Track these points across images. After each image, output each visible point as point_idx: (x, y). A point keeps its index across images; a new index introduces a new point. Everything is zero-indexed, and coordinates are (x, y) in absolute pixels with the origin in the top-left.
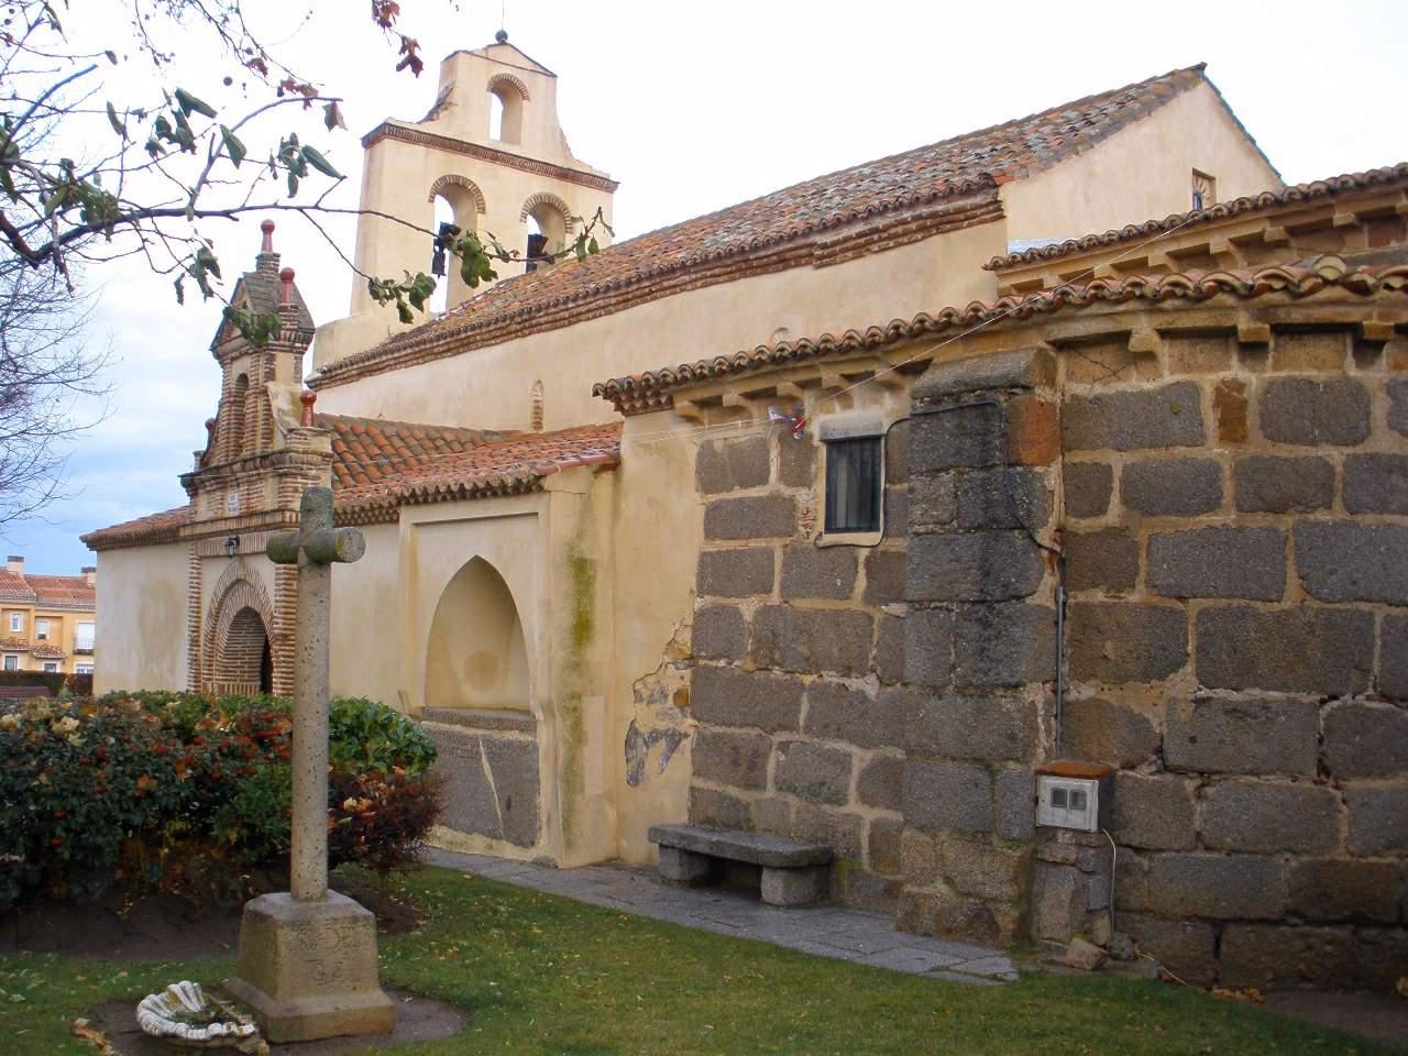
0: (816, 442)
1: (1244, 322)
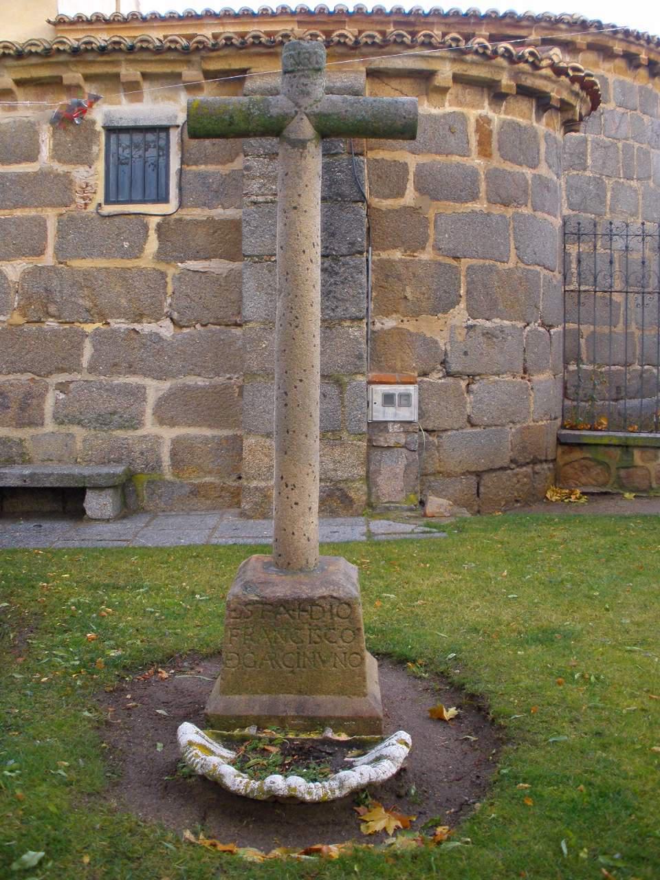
0: (99, 127)
1: (506, 81)
